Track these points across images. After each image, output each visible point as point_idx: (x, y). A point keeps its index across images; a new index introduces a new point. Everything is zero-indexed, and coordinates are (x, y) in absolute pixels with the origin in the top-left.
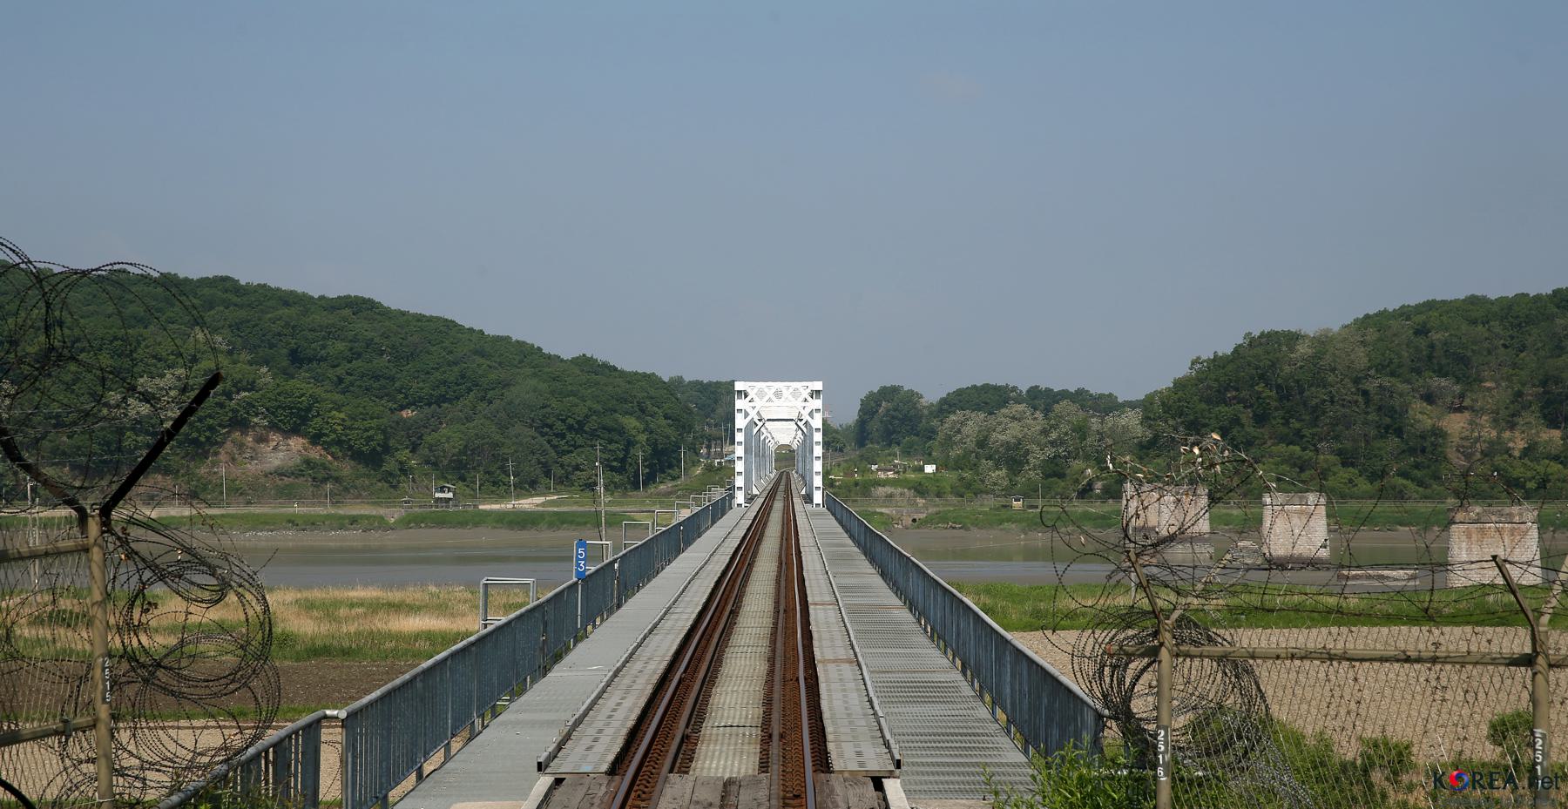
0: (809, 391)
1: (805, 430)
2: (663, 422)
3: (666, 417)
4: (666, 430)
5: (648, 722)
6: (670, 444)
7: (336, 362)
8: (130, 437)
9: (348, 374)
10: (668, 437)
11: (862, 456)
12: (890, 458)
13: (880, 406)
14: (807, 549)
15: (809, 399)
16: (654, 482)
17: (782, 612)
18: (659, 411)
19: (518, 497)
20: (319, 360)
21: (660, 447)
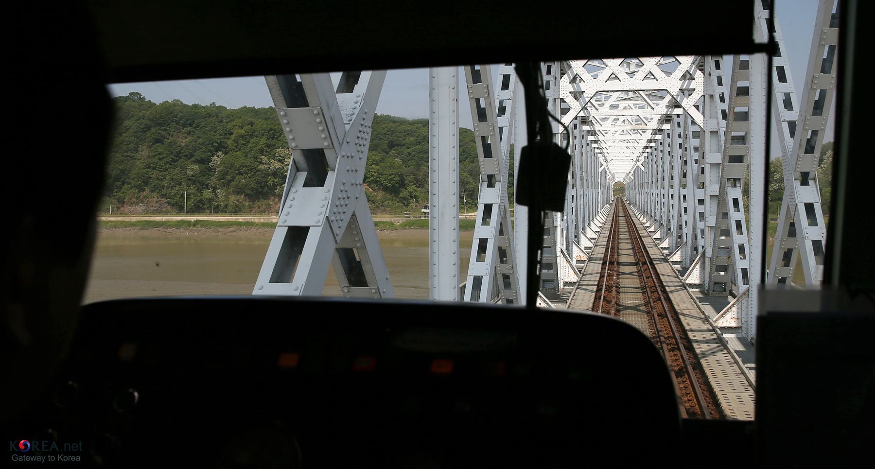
7: (409, 146)
8: (271, 179)
9: (413, 151)
19: (468, 212)
20: (402, 146)
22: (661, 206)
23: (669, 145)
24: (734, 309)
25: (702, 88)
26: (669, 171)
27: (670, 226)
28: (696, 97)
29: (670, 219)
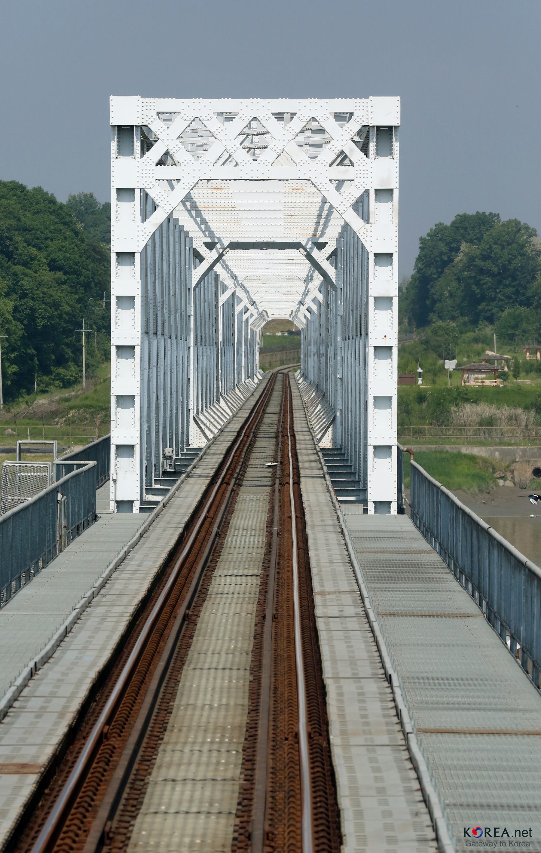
0: (354, 127)
1: (331, 271)
2: (47, 276)
3: (53, 266)
4: (52, 292)
5: (33, 834)
6: (60, 317)
10: (56, 305)
11: (426, 342)
12: (478, 347)
13: (457, 250)
14: (335, 624)
15: (356, 154)
16: (29, 392)
17: (269, 617)
18: (41, 255)
21: (41, 323)
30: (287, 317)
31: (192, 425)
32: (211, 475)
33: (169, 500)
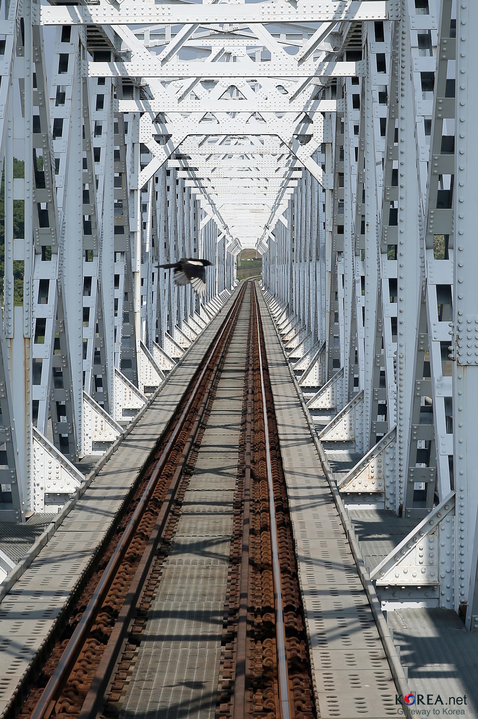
22: (354, 320)
23: (383, 97)
24: (373, 462)
25: (322, 134)
26: (354, 205)
27: (385, 396)
28: (314, 145)
29: (383, 373)
30: (253, 246)
31: (201, 308)
32: (157, 437)
33: (111, 454)
